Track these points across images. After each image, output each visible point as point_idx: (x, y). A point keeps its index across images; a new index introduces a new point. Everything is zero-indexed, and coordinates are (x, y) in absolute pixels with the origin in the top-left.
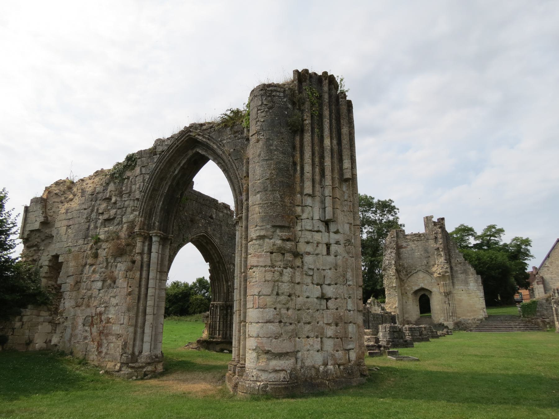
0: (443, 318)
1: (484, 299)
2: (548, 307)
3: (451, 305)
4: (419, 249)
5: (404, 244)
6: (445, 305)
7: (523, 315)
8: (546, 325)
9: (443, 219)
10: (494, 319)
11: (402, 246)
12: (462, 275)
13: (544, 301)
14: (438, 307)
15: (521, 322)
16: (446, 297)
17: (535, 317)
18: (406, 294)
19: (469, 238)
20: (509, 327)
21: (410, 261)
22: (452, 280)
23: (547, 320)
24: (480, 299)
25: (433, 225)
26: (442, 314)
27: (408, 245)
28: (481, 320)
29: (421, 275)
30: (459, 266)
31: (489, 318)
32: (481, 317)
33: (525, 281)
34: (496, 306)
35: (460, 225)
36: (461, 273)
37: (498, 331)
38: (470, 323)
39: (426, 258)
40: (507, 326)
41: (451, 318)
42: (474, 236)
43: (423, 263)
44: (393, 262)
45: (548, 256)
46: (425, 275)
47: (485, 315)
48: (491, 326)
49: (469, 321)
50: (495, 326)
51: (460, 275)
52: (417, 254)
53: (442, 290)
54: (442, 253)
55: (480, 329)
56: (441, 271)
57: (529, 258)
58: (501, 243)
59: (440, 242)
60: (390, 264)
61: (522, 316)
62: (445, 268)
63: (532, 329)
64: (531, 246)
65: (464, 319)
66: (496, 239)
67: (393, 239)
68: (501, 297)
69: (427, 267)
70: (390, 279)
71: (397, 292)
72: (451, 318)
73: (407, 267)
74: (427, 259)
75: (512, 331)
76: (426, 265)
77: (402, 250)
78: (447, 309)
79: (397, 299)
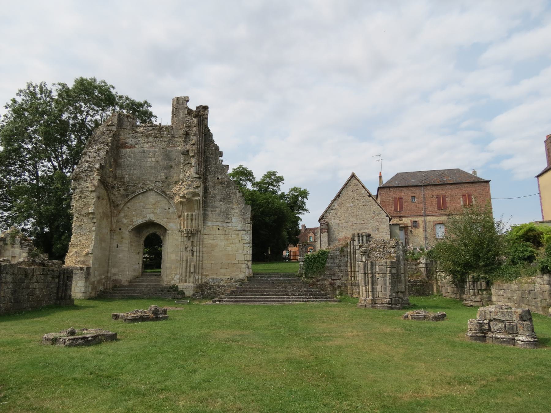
0: (178, 276)
1: (251, 245)
2: (341, 262)
3: (195, 254)
4: (156, 152)
5: (131, 141)
6: (185, 252)
7: (306, 274)
8: (336, 290)
9: (206, 108)
10: (263, 280)
11: (126, 143)
12: (221, 203)
13: (338, 253)
14: (173, 257)
15: (302, 285)
16: (189, 239)
17: (322, 276)
18: (120, 231)
19: (247, 184)
20: (284, 295)
21: (136, 171)
22: (204, 210)
23: (338, 282)
24: (245, 245)
25: (186, 113)
26: (178, 269)
27: (136, 143)
28: (242, 281)
29: (152, 198)
30: (220, 187)
31: (253, 277)
32: (241, 276)
33: (295, 238)
34: (264, 261)
35: (238, 166)
36: (221, 200)
37: (264, 301)
38: (222, 286)
39: (166, 168)
40: (279, 291)
41: (192, 276)
42: (252, 182)
43: (159, 178)
44: (97, 166)
45: (339, 195)
46: (159, 198)
47: (249, 273)
48: (256, 292)
49: (222, 283)
50: (262, 291)
51: (218, 204)
52: (151, 161)
53: (183, 228)
54: (193, 161)
55: (236, 298)
56: (185, 192)
57: (303, 212)
58: (279, 193)
59: (193, 142)
60: (90, 169)
61: (304, 276)
62: (194, 186)
63: (317, 298)
64: (308, 199)
65: (213, 279)
66: (275, 188)
67: (110, 128)
68: (271, 251)
69: (165, 184)
70: (85, 198)
71: (96, 224)
72: (192, 276)
73: (129, 183)
74: (166, 171)
75: (287, 301)
76: (163, 182)
77: (124, 151)
78: (187, 260)
79: (94, 237)
